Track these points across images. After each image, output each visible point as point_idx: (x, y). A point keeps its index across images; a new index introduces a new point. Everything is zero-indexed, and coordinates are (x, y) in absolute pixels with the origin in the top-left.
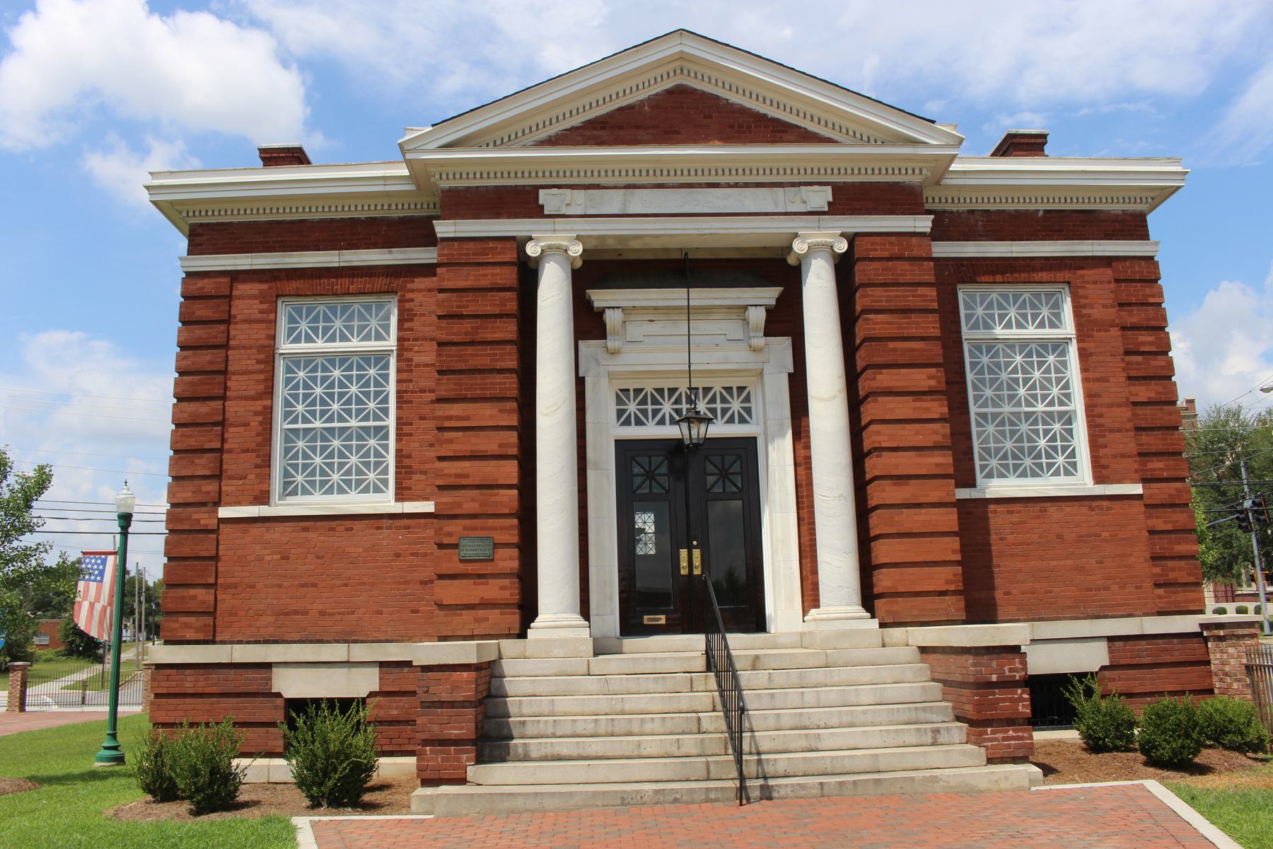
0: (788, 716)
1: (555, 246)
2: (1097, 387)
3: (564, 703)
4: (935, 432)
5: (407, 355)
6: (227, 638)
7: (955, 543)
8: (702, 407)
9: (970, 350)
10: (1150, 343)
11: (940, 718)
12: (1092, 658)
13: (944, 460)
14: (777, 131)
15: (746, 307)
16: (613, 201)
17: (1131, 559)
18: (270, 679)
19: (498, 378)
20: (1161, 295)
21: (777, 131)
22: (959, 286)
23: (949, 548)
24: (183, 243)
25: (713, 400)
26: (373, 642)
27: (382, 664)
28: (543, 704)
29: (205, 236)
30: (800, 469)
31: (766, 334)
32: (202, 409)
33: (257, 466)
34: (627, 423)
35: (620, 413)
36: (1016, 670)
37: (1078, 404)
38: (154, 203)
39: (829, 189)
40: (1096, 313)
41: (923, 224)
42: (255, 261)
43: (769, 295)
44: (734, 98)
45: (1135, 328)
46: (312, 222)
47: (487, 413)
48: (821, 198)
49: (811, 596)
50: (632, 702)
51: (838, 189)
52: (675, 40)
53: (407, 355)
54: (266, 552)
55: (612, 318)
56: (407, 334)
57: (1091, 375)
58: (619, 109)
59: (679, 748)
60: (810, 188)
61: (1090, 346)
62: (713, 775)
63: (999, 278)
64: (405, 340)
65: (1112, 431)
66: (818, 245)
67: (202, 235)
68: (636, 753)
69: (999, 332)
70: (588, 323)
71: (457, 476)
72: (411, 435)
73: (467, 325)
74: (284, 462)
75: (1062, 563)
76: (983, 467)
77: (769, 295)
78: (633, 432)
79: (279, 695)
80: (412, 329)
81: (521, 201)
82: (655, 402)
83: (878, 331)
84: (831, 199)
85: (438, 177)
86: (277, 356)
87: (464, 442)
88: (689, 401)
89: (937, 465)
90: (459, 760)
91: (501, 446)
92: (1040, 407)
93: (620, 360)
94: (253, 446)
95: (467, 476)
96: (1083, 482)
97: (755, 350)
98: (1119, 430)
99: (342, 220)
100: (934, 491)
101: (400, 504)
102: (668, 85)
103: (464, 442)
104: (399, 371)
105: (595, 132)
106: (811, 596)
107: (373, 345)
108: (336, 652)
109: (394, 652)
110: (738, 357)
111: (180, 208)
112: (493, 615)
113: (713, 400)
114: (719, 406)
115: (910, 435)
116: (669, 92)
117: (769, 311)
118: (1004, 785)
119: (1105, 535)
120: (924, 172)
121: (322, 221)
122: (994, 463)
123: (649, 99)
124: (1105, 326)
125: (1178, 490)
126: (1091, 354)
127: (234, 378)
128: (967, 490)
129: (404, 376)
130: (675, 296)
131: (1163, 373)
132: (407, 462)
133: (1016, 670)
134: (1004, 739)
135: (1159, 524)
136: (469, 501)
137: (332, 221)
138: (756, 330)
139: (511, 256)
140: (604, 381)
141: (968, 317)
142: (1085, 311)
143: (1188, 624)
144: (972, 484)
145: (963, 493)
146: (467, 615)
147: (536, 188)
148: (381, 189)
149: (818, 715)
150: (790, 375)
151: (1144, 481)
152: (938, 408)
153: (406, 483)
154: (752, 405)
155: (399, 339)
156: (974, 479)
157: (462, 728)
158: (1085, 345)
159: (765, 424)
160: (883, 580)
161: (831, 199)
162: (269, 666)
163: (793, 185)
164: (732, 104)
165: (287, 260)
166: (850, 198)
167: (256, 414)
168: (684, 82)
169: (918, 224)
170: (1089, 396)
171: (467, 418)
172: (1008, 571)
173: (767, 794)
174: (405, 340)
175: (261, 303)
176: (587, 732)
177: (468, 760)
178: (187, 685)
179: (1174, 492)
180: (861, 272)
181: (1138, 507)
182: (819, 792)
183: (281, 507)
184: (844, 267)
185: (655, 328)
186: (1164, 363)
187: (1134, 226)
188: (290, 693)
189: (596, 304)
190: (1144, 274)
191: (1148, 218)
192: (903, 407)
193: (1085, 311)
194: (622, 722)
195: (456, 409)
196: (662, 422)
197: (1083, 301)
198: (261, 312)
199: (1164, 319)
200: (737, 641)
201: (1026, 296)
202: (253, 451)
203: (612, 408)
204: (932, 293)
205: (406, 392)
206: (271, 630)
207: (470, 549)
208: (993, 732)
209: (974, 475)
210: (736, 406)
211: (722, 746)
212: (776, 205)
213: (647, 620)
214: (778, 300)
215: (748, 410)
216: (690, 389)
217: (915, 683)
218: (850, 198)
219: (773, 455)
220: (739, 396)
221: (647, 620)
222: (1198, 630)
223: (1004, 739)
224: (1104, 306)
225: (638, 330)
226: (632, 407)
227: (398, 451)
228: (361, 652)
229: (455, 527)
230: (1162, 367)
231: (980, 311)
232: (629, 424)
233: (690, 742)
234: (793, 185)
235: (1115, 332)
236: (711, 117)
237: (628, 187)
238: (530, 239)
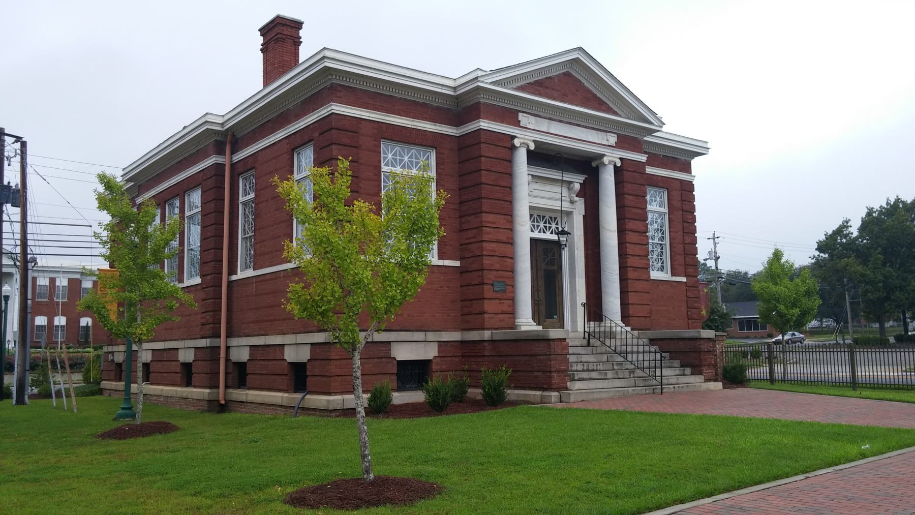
12: (428, 352)
22: (648, 189)
27: (312, 344)
41: (643, 158)
63: (545, 152)
71: (492, 251)
78: (537, 235)
95: (495, 251)
108: (419, 336)
116: (564, 74)
162: (178, 349)
171: (494, 223)
187: (687, 168)
190: (687, 188)
218: (625, 142)
228: (431, 336)
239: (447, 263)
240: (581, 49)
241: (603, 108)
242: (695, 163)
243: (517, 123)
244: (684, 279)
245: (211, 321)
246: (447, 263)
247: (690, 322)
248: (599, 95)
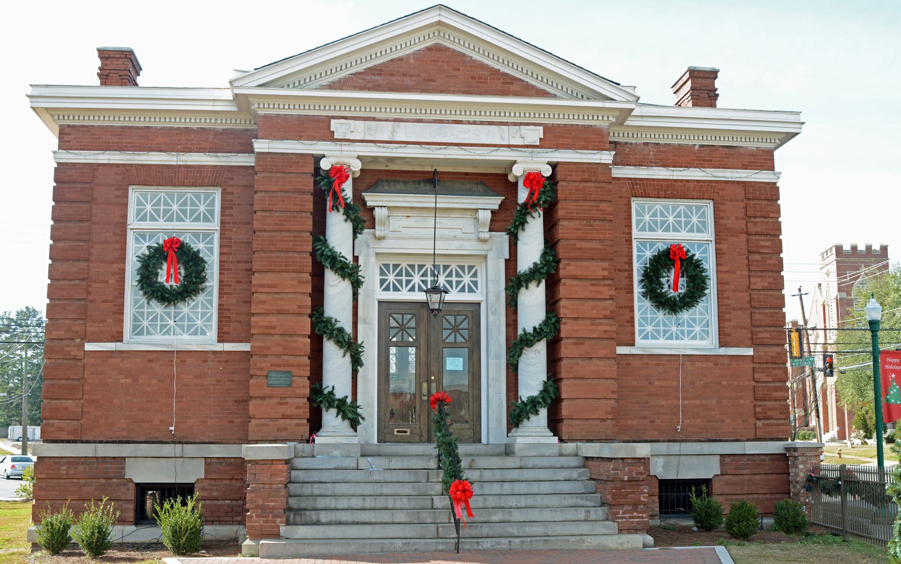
2: (726, 276)
4: (605, 308)
5: (227, 234)
6: (91, 438)
8: (442, 280)
9: (638, 246)
10: (767, 247)
11: (593, 504)
14: (505, 84)
15: (476, 210)
16: (384, 131)
17: (742, 402)
18: (124, 468)
20: (778, 212)
21: (505, 84)
22: (633, 199)
24: (55, 142)
25: (450, 275)
26: (200, 443)
29: (70, 137)
30: (511, 329)
31: (490, 230)
32: (74, 268)
33: (114, 313)
34: (387, 289)
35: (382, 282)
36: (642, 474)
38: (33, 108)
39: (541, 128)
41: (606, 157)
42: (112, 157)
43: (495, 202)
46: (156, 128)
48: (534, 135)
51: (547, 128)
52: (435, 13)
53: (227, 234)
54: (121, 376)
56: (228, 219)
57: (724, 268)
58: (392, 60)
60: (527, 127)
61: (724, 247)
62: (441, 535)
64: (226, 223)
65: (735, 309)
67: (69, 134)
68: (390, 520)
71: (267, 327)
72: (230, 294)
74: (133, 311)
75: (692, 402)
76: (641, 332)
77: (495, 202)
78: (391, 296)
79: (131, 480)
80: (231, 215)
82: (408, 274)
84: (542, 136)
85: (256, 106)
86: (128, 231)
88: (433, 275)
89: (605, 331)
90: (275, 522)
91: (299, 307)
93: (384, 243)
94: (111, 298)
97: (484, 241)
98: (740, 309)
99: (179, 129)
101: (221, 344)
102: (429, 44)
104: (221, 246)
105: (373, 77)
110: (471, 247)
111: (53, 113)
113: (450, 275)
114: (454, 279)
116: (429, 49)
117: (493, 212)
118: (626, 546)
119: (724, 383)
120: (611, 119)
121: (163, 128)
122: (649, 328)
123: (414, 53)
124: (735, 233)
125: (778, 354)
126: (724, 253)
127: (96, 246)
128: (628, 348)
129: (225, 250)
130: (427, 200)
131: (775, 269)
132: (227, 314)
133: (642, 474)
134: (630, 518)
137: (171, 128)
138: (484, 225)
140: (373, 259)
141: (638, 222)
142: (723, 222)
144: (632, 344)
148: (211, 108)
150: (506, 260)
153: (226, 329)
154: (479, 279)
155: (223, 223)
156: (634, 340)
157: (276, 501)
158: (719, 246)
159: (487, 294)
161: (542, 136)
163: (515, 124)
164: (475, 61)
165: (137, 157)
167: (113, 274)
168: (440, 42)
169: (604, 157)
171: (275, 286)
174: (226, 223)
175: (117, 190)
176: (358, 507)
177: (281, 522)
178: (61, 472)
179: (775, 355)
182: (508, 547)
183: (131, 342)
185: (411, 222)
186: (775, 262)
187: (765, 161)
188: (138, 480)
189: (369, 204)
191: (776, 153)
193: (723, 222)
196: (412, 289)
197: (722, 214)
198: (117, 197)
199: (780, 229)
201: (682, 208)
202: (110, 302)
203: (378, 278)
205: (227, 262)
206: (124, 434)
208: (623, 513)
209: (634, 337)
210: (467, 279)
211: (447, 517)
212: (502, 139)
214: (500, 206)
215: (475, 283)
216: (434, 266)
220: (469, 273)
222: (783, 452)
223: (630, 518)
224: (737, 218)
225: (398, 223)
227: (220, 306)
230: (775, 265)
232: (389, 290)
234: (515, 124)
236: (459, 70)
237: (395, 120)
238: (324, 156)
239: (229, 347)
240: (441, 7)
241: (514, 88)
242: (779, 155)
243: (330, 137)
244: (750, 352)
245: (252, 403)
246: (229, 347)
247: (759, 424)
248: (503, 69)
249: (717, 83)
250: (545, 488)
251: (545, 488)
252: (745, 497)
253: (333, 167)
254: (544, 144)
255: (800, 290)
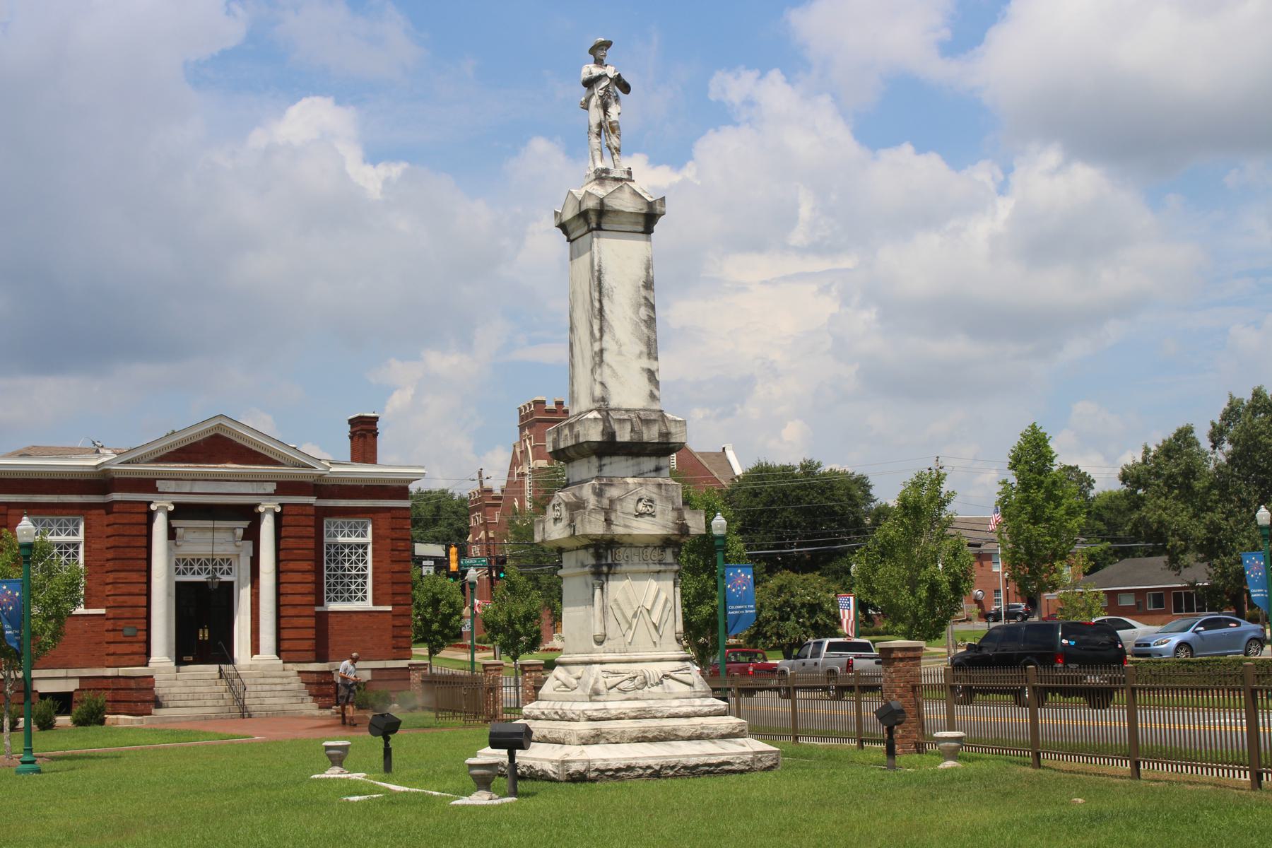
0: (253, 695)
1: (161, 505)
3: (174, 690)
7: (313, 631)
13: (312, 598)
16: (186, 487)
19: (139, 562)
23: (311, 633)
28: (166, 690)
37: (369, 571)
40: (381, 532)
43: (245, 524)
44: (239, 441)
45: (397, 539)
47: (134, 577)
48: (271, 488)
49: (255, 649)
50: (198, 689)
55: (179, 532)
59: (608, 521)
66: (268, 508)
69: (340, 539)
70: (172, 534)
73: (126, 539)
77: (245, 524)
81: (147, 485)
83: (290, 546)
87: (124, 589)
92: (354, 572)
96: (368, 605)
100: (308, 611)
103: (124, 589)
106: (255, 649)
107: (71, 539)
109: (87, 672)
112: (136, 657)
115: (299, 588)
122: (332, 595)
135: (397, 623)
136: (127, 613)
139: (144, 510)
143: (403, 664)
144: (322, 604)
145: (318, 609)
146: (126, 658)
147: (156, 479)
149: (263, 694)
151: (393, 605)
152: (311, 578)
160: (285, 645)
166: (284, 488)
170: (374, 568)
172: (334, 640)
173: (250, 716)
180: (285, 520)
181: (390, 616)
184: (278, 517)
188: (41, 691)
192: (297, 577)
194: (196, 696)
195: (122, 575)
200: (225, 667)
204: (313, 530)
207: (128, 632)
210: (225, 567)
213: (185, 658)
217: (296, 683)
219: (242, 592)
221: (185, 658)
225: (190, 536)
226: (181, 567)
228: (72, 673)
229: (122, 622)
231: (332, 529)
233: (222, 702)
235: (389, 541)
244: (390, 608)
249: (379, 424)
250: (279, 688)
251: (279, 688)
252: (596, 657)
253: (375, 735)
254: (278, 493)
255: (480, 474)
